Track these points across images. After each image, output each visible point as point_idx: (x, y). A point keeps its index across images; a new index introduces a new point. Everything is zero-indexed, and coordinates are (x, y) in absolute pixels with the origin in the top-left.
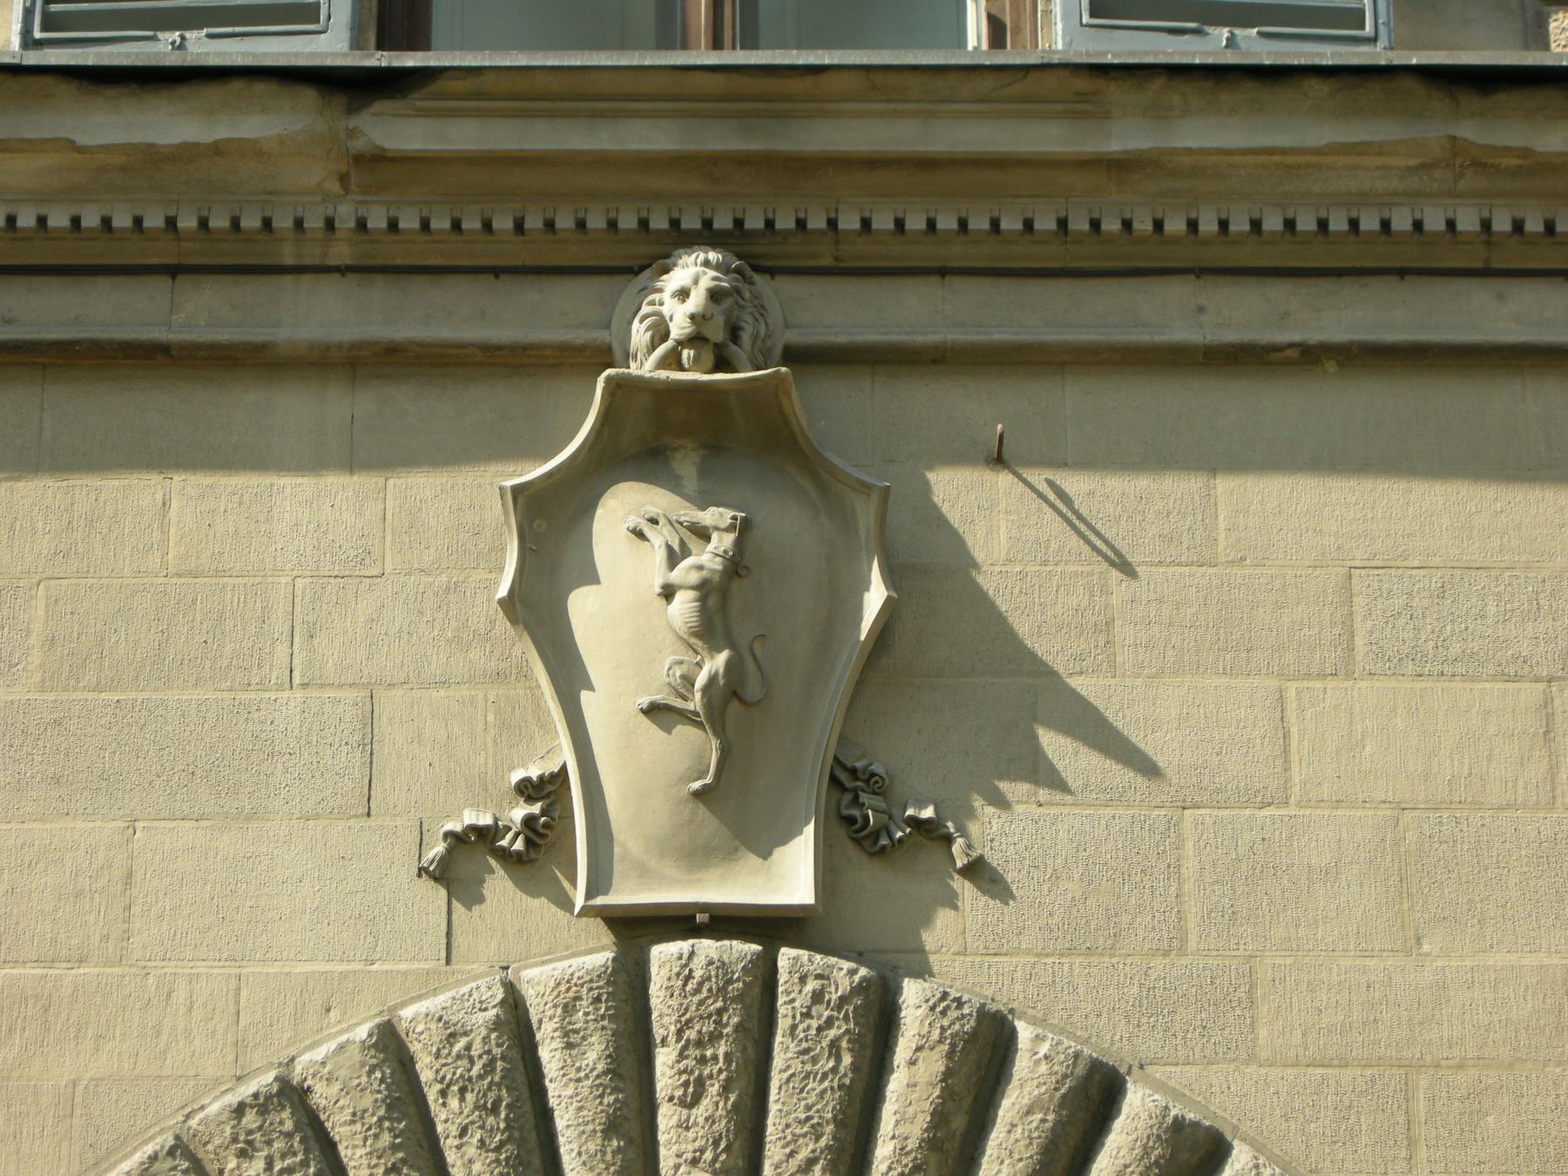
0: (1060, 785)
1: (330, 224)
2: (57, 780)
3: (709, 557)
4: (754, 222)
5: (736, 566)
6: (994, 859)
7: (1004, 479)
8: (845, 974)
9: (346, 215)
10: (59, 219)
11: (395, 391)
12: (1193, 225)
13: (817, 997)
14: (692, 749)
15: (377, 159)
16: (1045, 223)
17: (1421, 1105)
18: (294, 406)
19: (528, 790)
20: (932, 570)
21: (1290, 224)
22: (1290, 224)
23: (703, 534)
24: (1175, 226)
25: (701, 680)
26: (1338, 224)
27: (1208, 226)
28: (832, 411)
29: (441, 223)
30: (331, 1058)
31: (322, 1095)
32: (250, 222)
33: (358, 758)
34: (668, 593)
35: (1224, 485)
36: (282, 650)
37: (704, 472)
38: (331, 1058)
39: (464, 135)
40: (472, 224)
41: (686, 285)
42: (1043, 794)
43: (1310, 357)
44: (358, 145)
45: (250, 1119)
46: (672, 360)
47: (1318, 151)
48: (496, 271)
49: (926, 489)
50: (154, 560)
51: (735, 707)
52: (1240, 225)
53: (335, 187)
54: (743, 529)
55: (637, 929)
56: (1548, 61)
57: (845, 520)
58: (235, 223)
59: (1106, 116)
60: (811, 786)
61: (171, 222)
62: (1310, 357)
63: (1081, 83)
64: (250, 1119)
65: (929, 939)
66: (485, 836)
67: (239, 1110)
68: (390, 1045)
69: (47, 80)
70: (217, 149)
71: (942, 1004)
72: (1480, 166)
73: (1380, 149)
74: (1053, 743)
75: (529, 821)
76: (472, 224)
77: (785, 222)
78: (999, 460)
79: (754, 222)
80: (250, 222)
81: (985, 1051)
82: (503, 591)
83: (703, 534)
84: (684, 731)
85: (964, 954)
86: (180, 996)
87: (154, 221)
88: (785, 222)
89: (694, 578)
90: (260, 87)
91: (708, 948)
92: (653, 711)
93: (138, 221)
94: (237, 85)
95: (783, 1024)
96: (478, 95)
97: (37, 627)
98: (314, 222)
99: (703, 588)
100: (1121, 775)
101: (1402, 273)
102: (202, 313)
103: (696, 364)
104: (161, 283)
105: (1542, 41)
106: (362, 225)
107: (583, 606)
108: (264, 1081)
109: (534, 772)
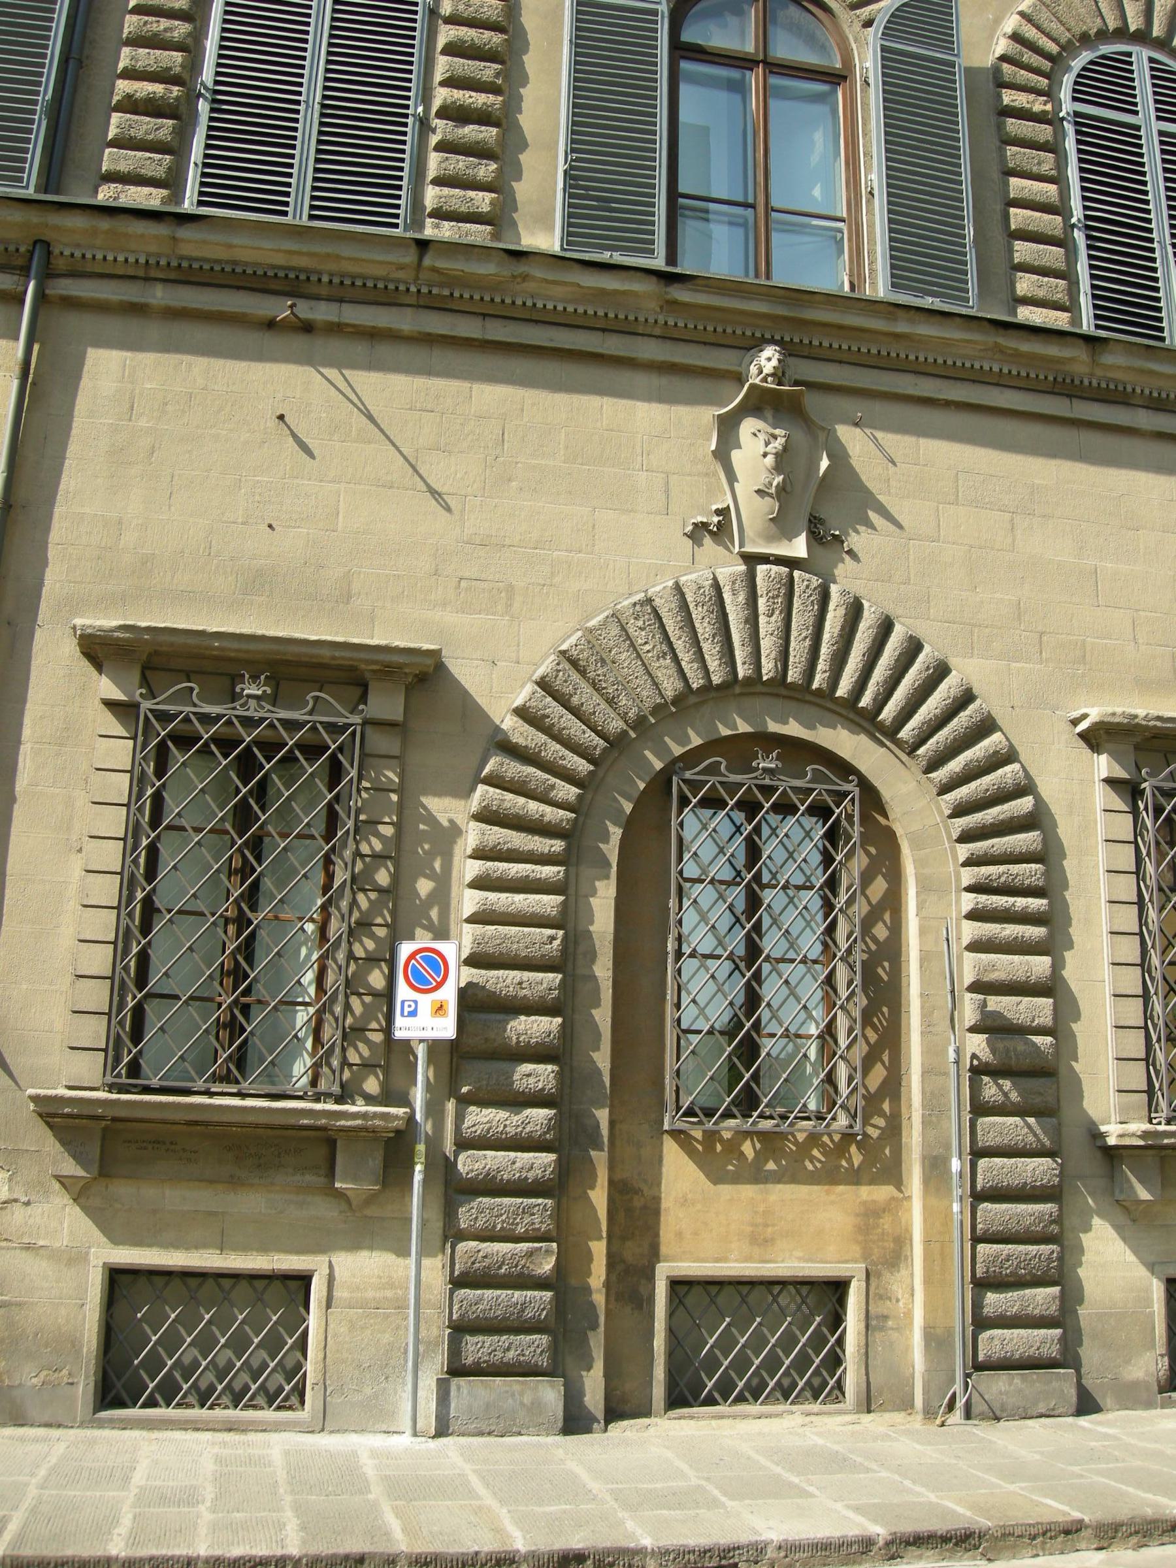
0: (875, 529)
1: (656, 322)
2: (570, 493)
3: (778, 444)
4: (787, 339)
5: (785, 448)
6: (855, 550)
7: (858, 430)
8: (816, 581)
9: (661, 321)
10: (570, 309)
11: (677, 378)
12: (917, 358)
13: (807, 587)
14: (769, 506)
15: (675, 302)
16: (874, 351)
17: (975, 638)
18: (642, 379)
19: (718, 512)
20: (839, 457)
21: (945, 362)
22: (945, 362)
23: (775, 437)
24: (912, 357)
25: (775, 484)
26: (959, 364)
27: (921, 359)
28: (813, 402)
29: (691, 326)
30: (661, 588)
31: (658, 602)
32: (631, 318)
33: (664, 497)
34: (765, 455)
35: (922, 441)
36: (639, 458)
37: (774, 417)
38: (661, 588)
39: (702, 299)
40: (700, 327)
41: (768, 359)
42: (869, 531)
43: (947, 404)
44: (668, 297)
45: (638, 608)
46: (765, 380)
47: (957, 341)
48: (705, 343)
49: (835, 431)
50: (599, 424)
51: (783, 493)
52: (931, 360)
53: (658, 309)
54: (788, 438)
55: (752, 560)
56: (1014, 320)
57: (815, 438)
58: (626, 317)
59: (896, 320)
60: (806, 523)
61: (606, 315)
62: (947, 404)
63: (891, 309)
64: (638, 608)
65: (836, 572)
66: (704, 526)
67: (635, 604)
68: (678, 589)
69: (572, 263)
70: (624, 293)
71: (844, 593)
72: (1001, 352)
73: (975, 342)
74: (871, 514)
75: (719, 522)
76: (700, 327)
77: (797, 340)
78: (856, 425)
79: (787, 339)
80: (631, 318)
81: (855, 611)
82: (713, 447)
83: (775, 437)
84: (767, 499)
85: (847, 579)
86: (611, 566)
87: (601, 313)
88: (797, 340)
89: (774, 451)
90: (639, 274)
91: (775, 568)
92: (758, 492)
93: (595, 313)
94: (632, 272)
95: (797, 594)
96: (706, 286)
97: (562, 442)
98: (651, 320)
99: (776, 454)
100: (892, 528)
101: (974, 381)
102: (613, 345)
103: (773, 383)
104: (600, 334)
105: (1015, 315)
106: (666, 323)
107: (736, 456)
108: (640, 596)
109: (720, 507)
